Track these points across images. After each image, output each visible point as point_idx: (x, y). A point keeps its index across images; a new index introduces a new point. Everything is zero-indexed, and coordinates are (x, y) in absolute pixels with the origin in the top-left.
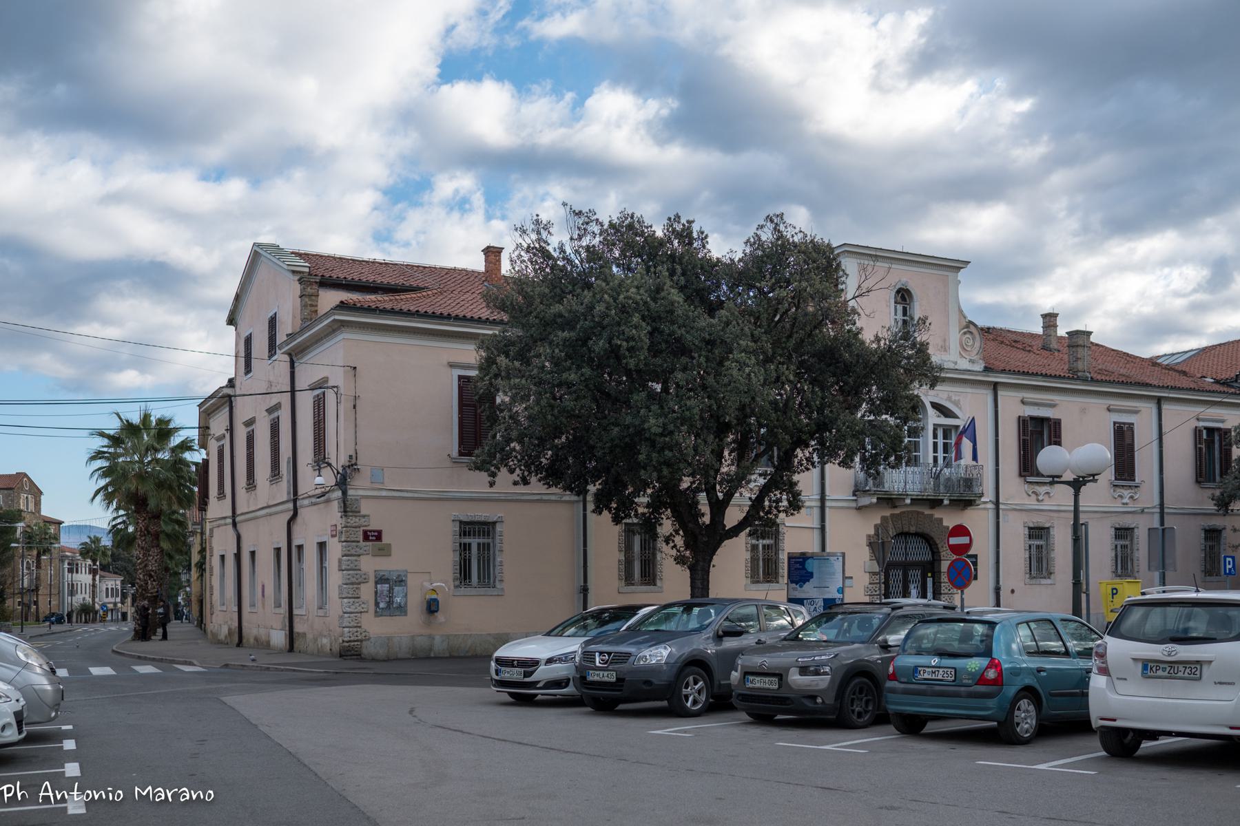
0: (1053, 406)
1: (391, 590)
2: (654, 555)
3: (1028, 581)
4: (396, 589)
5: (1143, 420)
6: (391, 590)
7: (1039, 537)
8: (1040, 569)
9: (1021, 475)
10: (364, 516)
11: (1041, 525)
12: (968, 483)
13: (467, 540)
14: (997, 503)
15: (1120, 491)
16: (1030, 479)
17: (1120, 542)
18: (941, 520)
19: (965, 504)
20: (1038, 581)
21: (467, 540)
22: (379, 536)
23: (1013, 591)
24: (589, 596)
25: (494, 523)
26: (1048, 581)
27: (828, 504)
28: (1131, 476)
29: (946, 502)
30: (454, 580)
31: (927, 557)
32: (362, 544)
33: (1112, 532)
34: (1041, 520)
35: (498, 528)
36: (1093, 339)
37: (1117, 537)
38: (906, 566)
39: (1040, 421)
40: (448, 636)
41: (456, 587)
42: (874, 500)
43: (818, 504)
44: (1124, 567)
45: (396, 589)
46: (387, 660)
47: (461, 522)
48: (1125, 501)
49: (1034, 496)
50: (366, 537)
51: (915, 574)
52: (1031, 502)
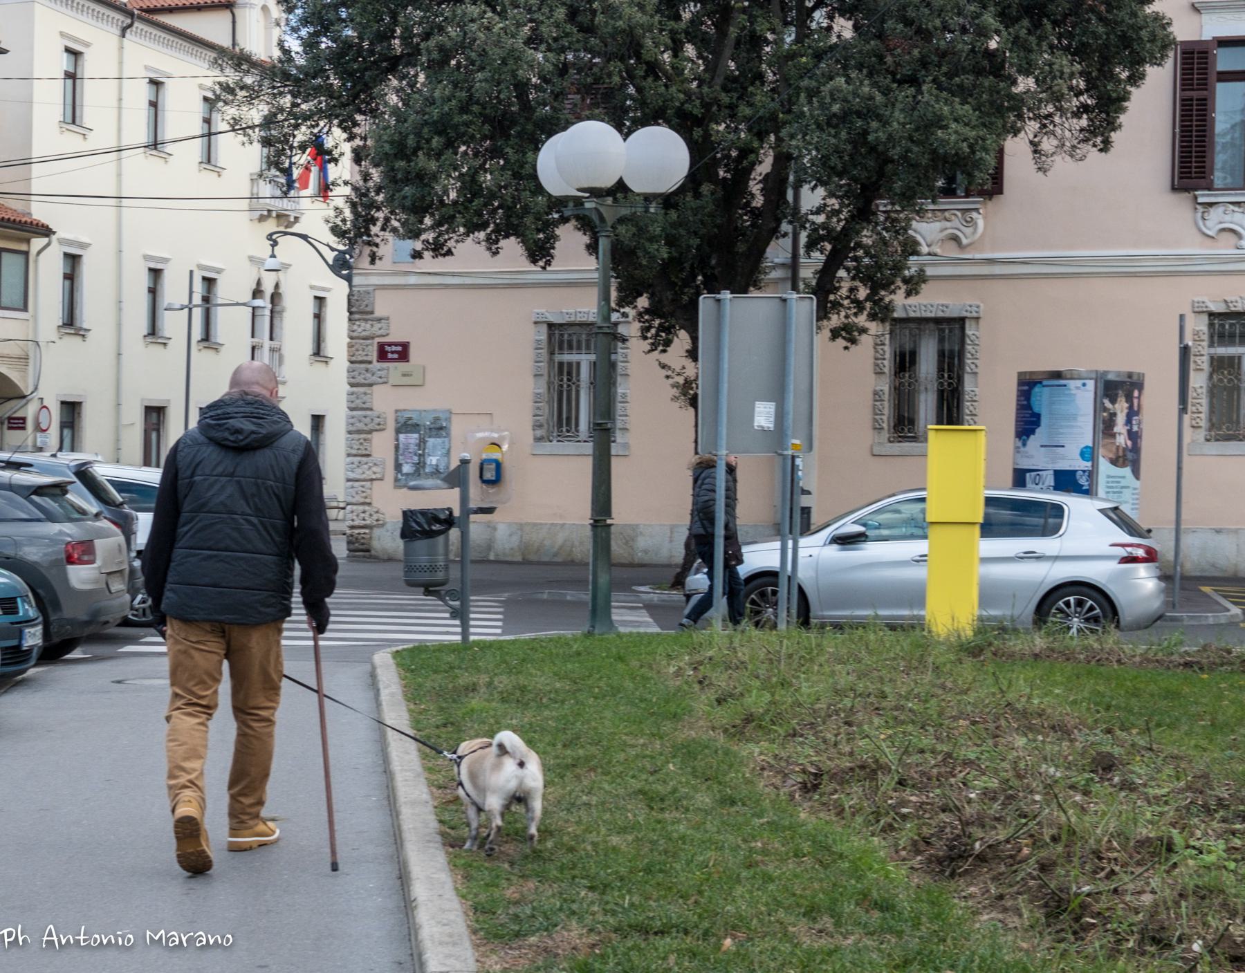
1: (422, 443)
2: (960, 380)
4: (431, 442)
6: (422, 443)
10: (379, 320)
13: (566, 357)
21: (566, 357)
22: (403, 353)
30: (538, 426)
32: (376, 365)
40: (521, 526)
41: (538, 439)
45: (431, 442)
46: (526, 562)
47: (551, 326)
50: (383, 355)
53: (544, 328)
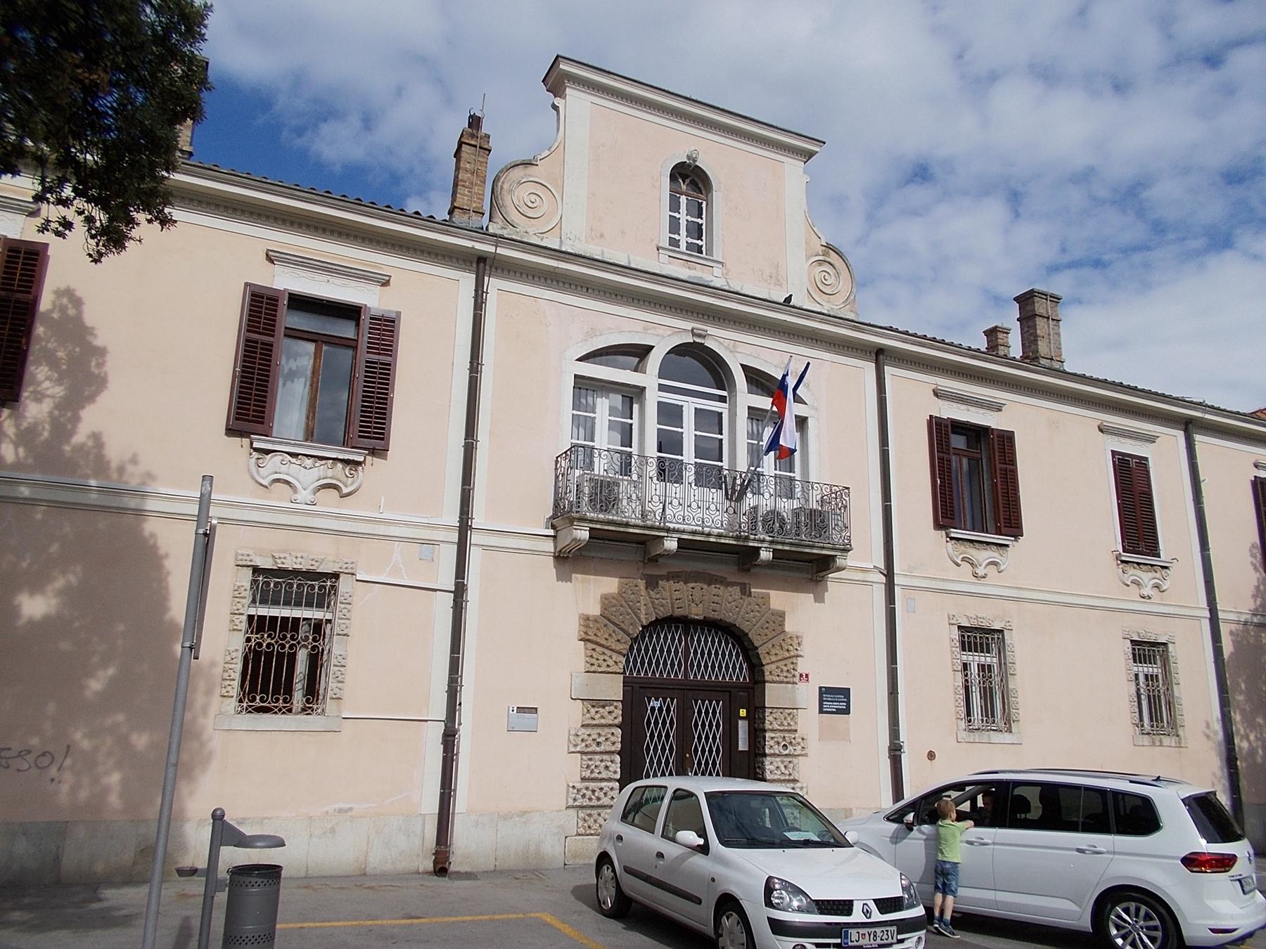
0: (998, 408)
3: (963, 735)
5: (1164, 454)
7: (983, 648)
8: (988, 711)
9: (938, 526)
11: (985, 624)
12: (817, 520)
14: (889, 573)
15: (1134, 573)
16: (955, 533)
17: (975, 659)
18: (766, 598)
19: (811, 567)
20: (985, 736)
23: (931, 756)
24: (905, 759)
25: (336, 576)
26: (1006, 738)
27: (474, 538)
28: (1153, 550)
29: (765, 555)
31: (737, 673)
33: (956, 633)
34: (988, 615)
35: (344, 585)
36: (205, 95)
37: (966, 646)
38: (687, 692)
39: (976, 434)
42: (584, 534)
43: (455, 537)
44: (1155, 716)
47: (256, 570)
48: (1146, 592)
49: (966, 566)
51: (709, 713)
52: (1130, 598)
53: (248, 574)
